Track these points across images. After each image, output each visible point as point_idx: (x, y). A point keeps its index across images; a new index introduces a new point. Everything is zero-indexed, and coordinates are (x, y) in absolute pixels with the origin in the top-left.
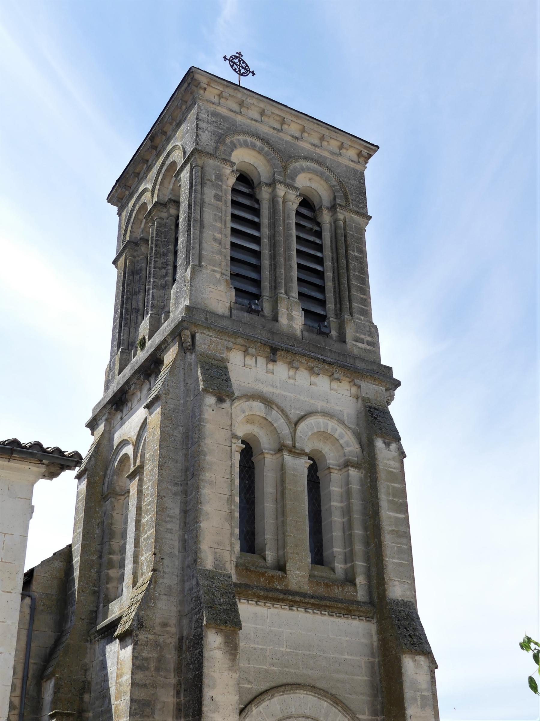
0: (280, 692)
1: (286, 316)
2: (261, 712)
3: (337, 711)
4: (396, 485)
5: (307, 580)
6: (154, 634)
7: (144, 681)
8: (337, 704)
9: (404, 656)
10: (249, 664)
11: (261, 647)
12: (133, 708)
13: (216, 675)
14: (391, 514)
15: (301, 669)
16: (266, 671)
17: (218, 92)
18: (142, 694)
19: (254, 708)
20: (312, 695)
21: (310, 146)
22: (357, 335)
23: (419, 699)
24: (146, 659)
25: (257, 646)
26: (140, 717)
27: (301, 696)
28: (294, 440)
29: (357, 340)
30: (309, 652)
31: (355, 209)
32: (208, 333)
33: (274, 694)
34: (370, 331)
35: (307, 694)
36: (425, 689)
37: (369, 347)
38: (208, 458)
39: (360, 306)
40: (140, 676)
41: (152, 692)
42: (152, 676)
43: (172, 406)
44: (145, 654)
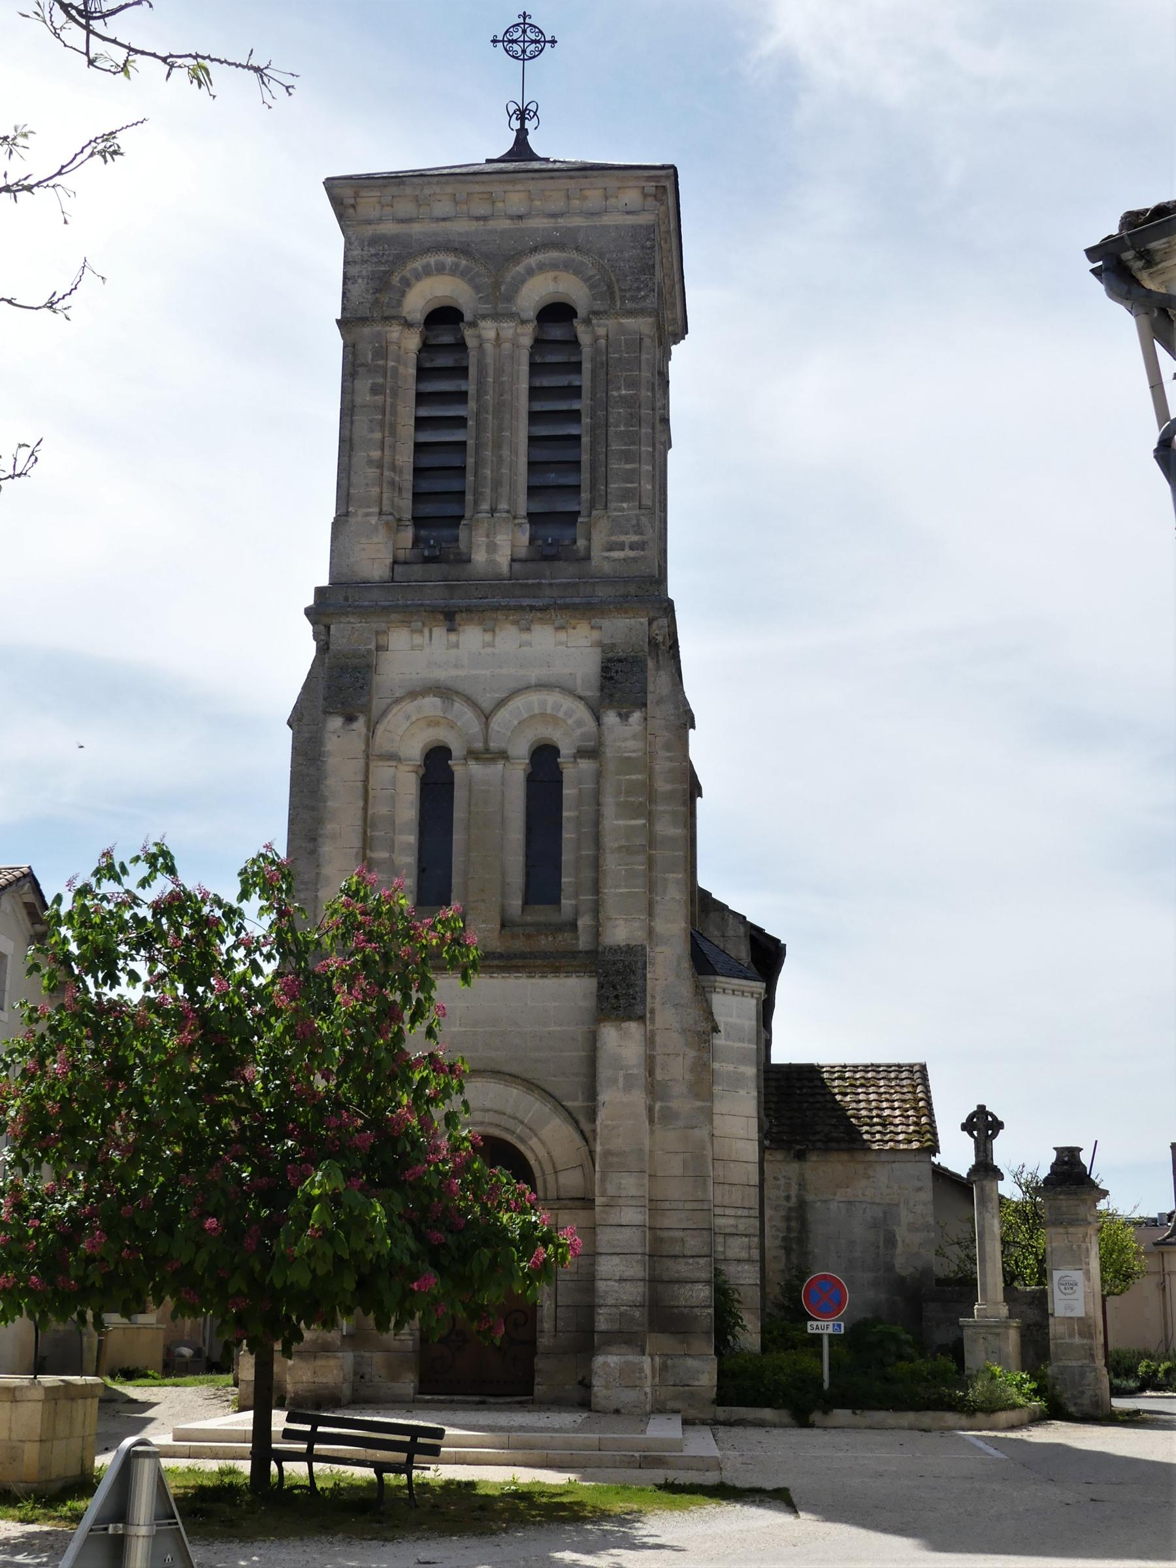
1: (484, 548)
4: (634, 777)
5: (496, 934)
14: (621, 822)
17: (375, 200)
21: (546, 220)
22: (613, 538)
23: (621, 1080)
28: (486, 741)
29: (611, 547)
31: (634, 305)
32: (348, 619)
34: (638, 525)
37: (632, 554)
38: (330, 803)
39: (622, 485)
43: (306, 735)
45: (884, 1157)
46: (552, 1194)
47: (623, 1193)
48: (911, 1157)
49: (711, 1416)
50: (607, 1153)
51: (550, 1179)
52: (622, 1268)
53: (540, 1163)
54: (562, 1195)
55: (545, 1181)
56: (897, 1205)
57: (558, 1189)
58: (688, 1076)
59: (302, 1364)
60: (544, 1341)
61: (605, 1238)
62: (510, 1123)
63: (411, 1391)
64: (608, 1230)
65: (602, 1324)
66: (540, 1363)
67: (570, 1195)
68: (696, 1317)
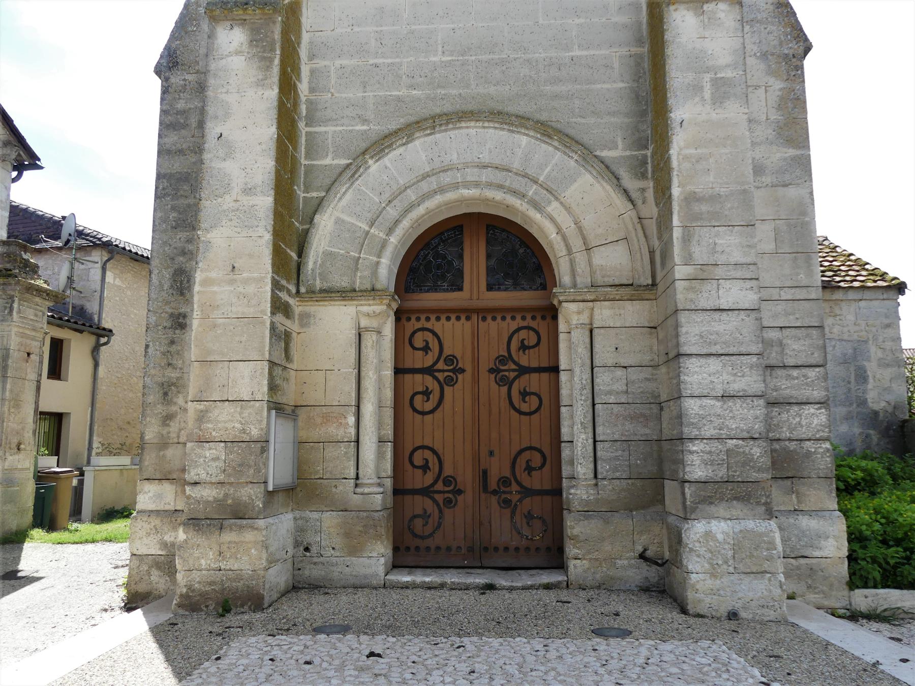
0: (427, 128)
2: (386, 167)
3: (551, 149)
6: (198, 72)
7: (178, 145)
8: (550, 137)
9: (672, 8)
10: (365, 92)
11: (390, 61)
12: (161, 187)
13: (232, 98)
15: (473, 87)
16: (399, 99)
18: (177, 165)
19: (371, 162)
20: (496, 128)
24: (183, 112)
25: (379, 61)
26: (172, 200)
27: (472, 132)
30: (491, 56)
33: (413, 134)
35: (484, 127)
36: (727, 66)
40: (172, 138)
41: (194, 160)
42: (193, 136)
44: (181, 105)
45: (851, 295)
46: (583, 279)
47: (722, 259)
48: (879, 295)
49: (845, 603)
50: (690, 199)
51: (581, 259)
52: (725, 377)
53: (564, 238)
54: (600, 280)
55: (572, 263)
56: (866, 342)
57: (592, 273)
58: (774, 116)
59: (199, 540)
60: (579, 492)
61: (692, 332)
62: (518, 183)
63: (381, 570)
64: (698, 317)
65: (697, 467)
66: (574, 526)
67: (610, 281)
68: (808, 454)
